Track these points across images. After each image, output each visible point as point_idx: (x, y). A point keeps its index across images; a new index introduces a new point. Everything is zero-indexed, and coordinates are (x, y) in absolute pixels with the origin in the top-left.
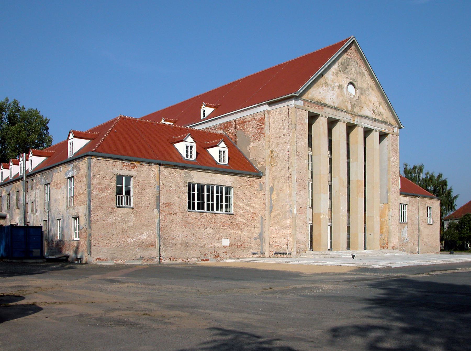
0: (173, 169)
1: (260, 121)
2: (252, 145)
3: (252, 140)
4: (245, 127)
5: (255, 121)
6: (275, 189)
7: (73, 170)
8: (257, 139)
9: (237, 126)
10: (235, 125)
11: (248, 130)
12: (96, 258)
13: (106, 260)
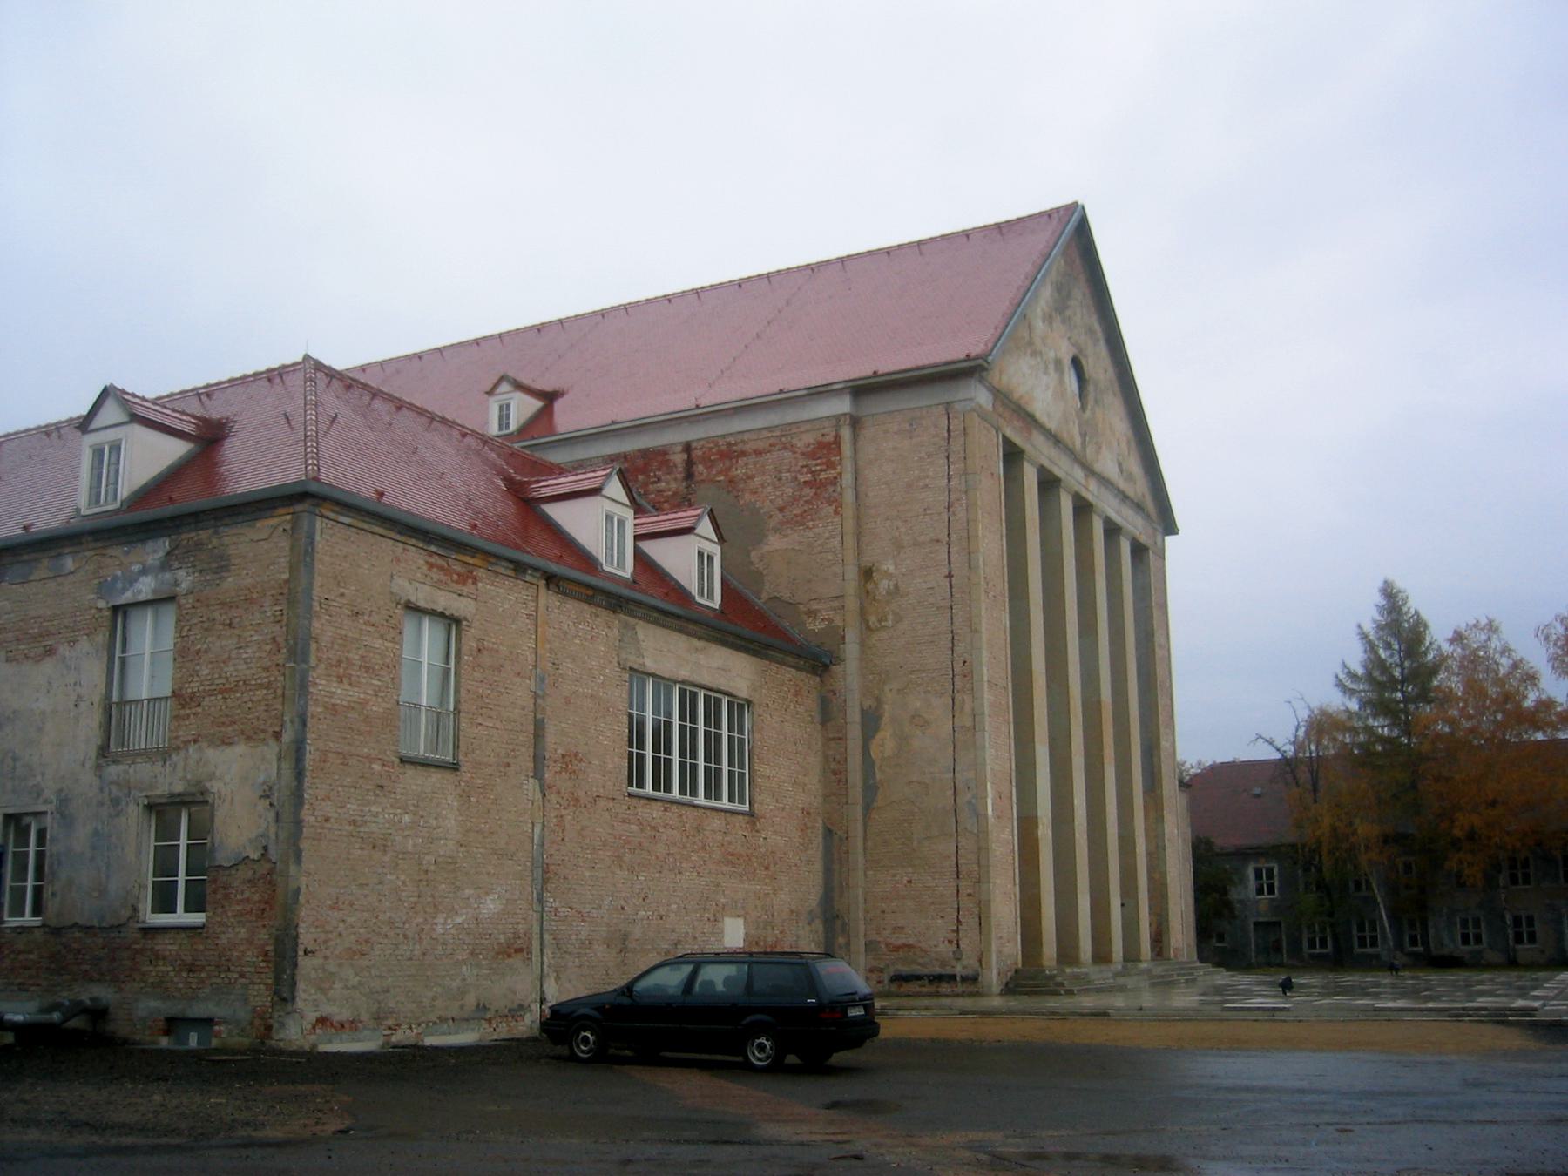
0: (586, 607)
1: (812, 455)
2: (775, 542)
3: (772, 523)
4: (739, 472)
5: (787, 454)
6: (886, 719)
7: (165, 566)
8: (800, 521)
9: (700, 468)
10: (689, 464)
11: (751, 485)
12: (312, 1016)
13: (353, 1025)
